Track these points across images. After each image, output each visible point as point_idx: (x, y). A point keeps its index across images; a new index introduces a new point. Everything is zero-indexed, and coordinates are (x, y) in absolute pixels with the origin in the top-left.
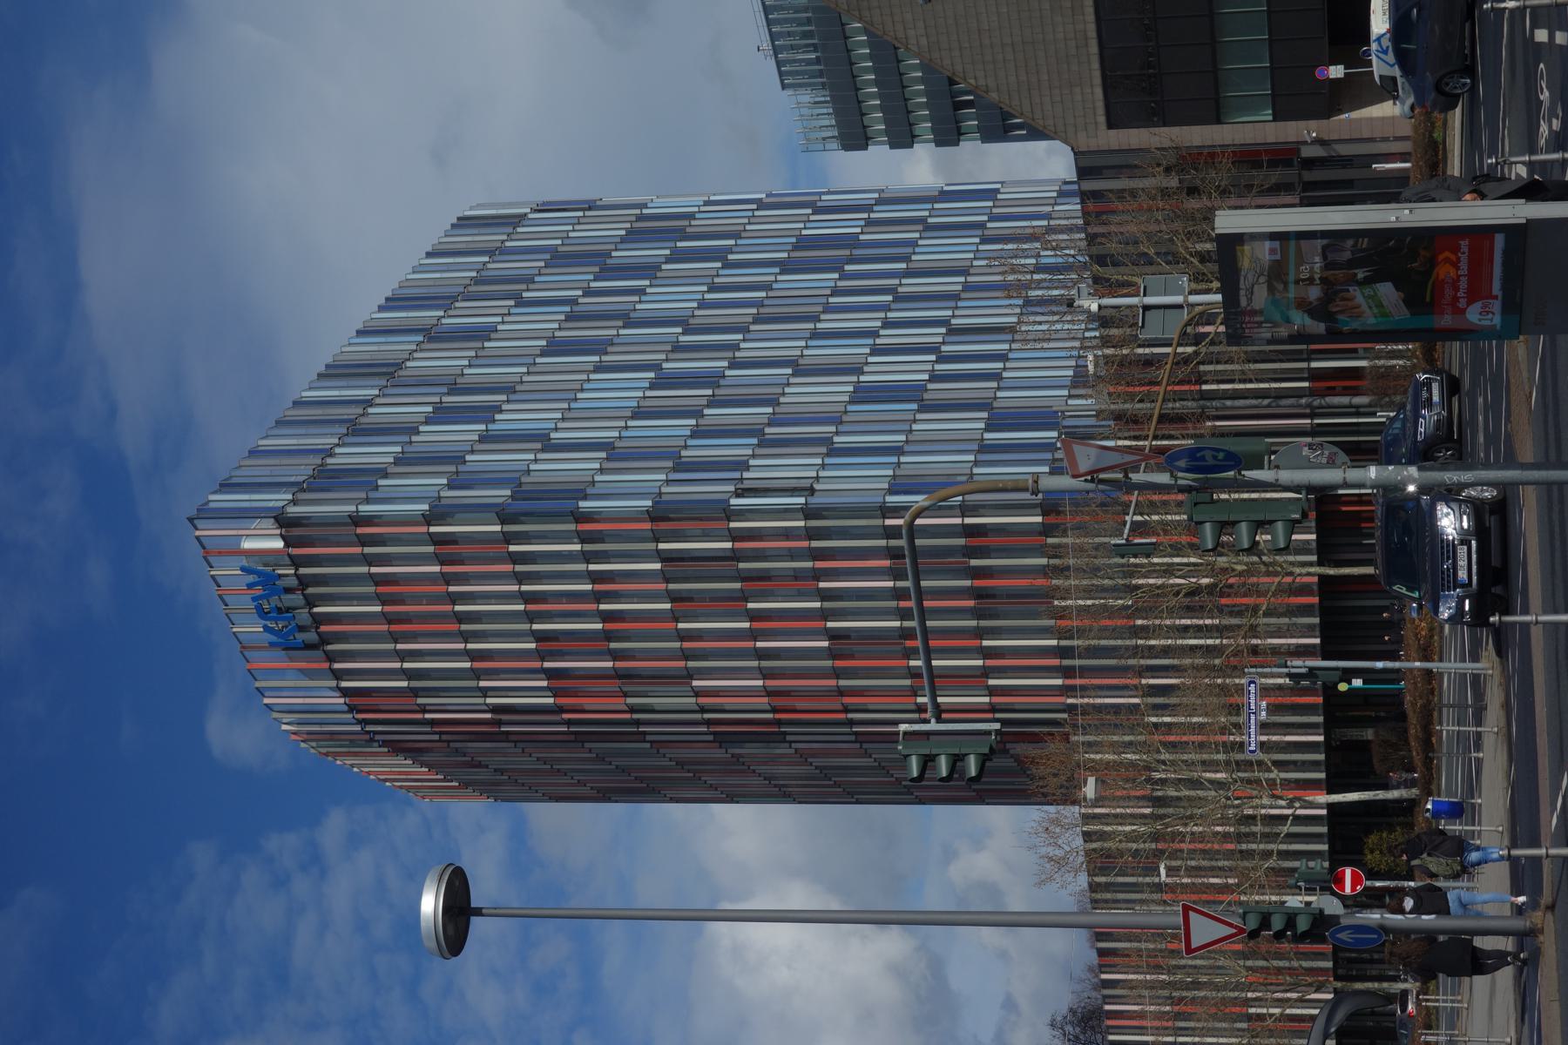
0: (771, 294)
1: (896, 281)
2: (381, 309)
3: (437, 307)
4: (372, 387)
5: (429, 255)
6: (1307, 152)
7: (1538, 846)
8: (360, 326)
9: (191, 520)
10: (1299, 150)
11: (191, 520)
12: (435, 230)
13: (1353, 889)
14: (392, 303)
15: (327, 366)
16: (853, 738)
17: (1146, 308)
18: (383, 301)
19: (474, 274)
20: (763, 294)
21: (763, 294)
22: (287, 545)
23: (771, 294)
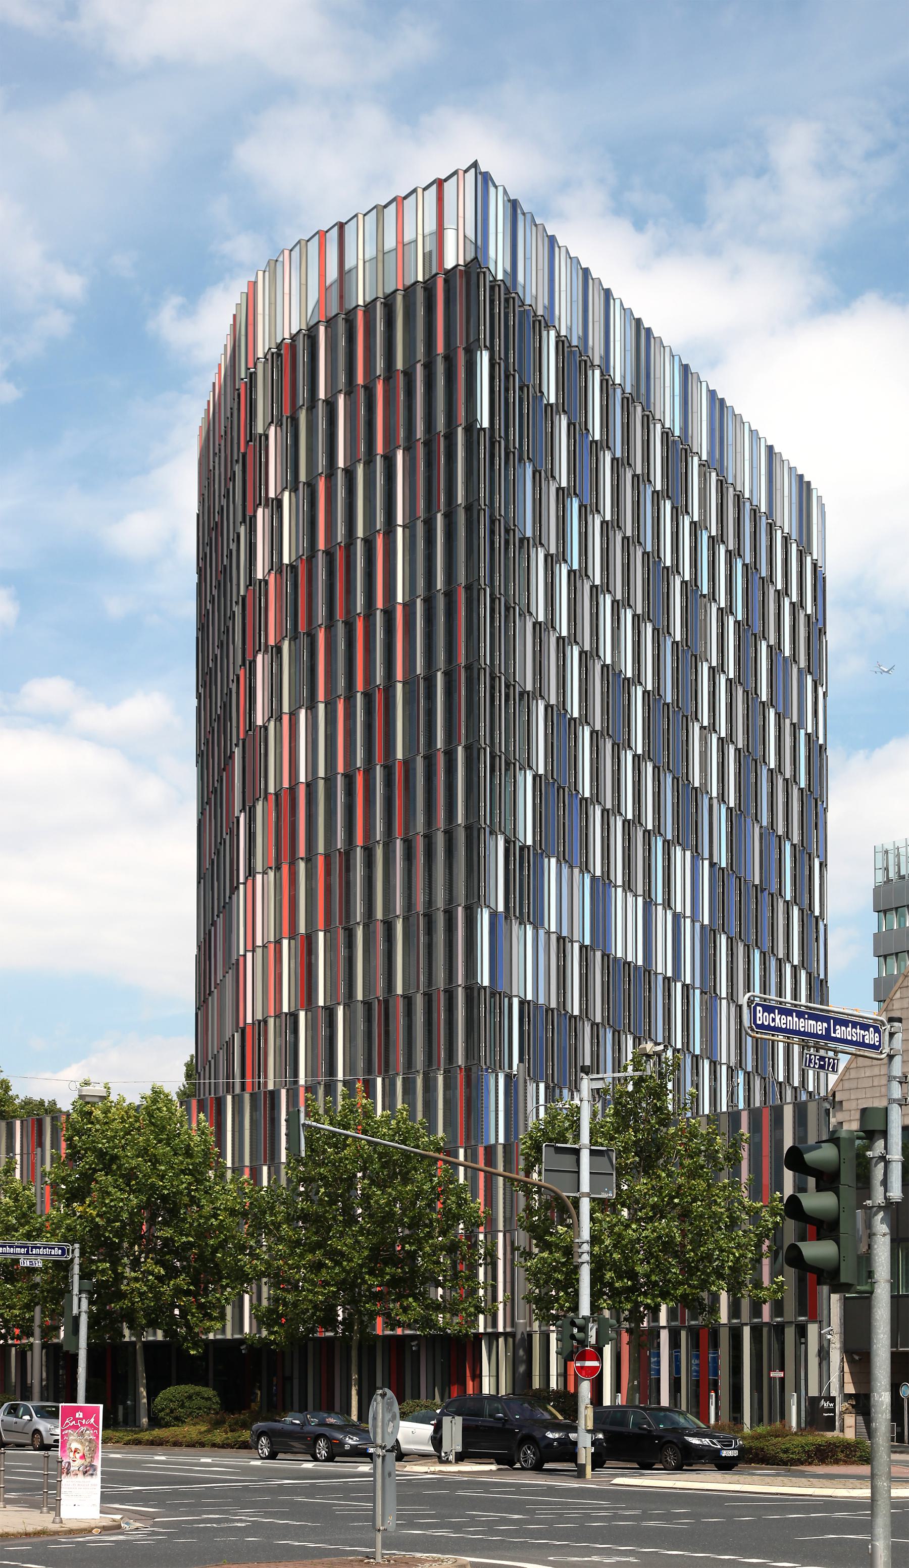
0: (715, 802)
1: (640, 891)
2: (712, 394)
3: (711, 453)
4: (624, 377)
5: (770, 449)
6: (812, 1330)
7: (383, 1547)
8: (777, 450)
9: (475, 165)
10: (815, 1322)
11: (475, 165)
12: (797, 455)
13: (614, 1398)
14: (718, 405)
15: (809, 483)
16: (250, 882)
17: (577, 1152)
18: (806, 479)
19: (747, 495)
20: (714, 794)
21: (714, 794)
22: (447, 273)
23: (715, 802)
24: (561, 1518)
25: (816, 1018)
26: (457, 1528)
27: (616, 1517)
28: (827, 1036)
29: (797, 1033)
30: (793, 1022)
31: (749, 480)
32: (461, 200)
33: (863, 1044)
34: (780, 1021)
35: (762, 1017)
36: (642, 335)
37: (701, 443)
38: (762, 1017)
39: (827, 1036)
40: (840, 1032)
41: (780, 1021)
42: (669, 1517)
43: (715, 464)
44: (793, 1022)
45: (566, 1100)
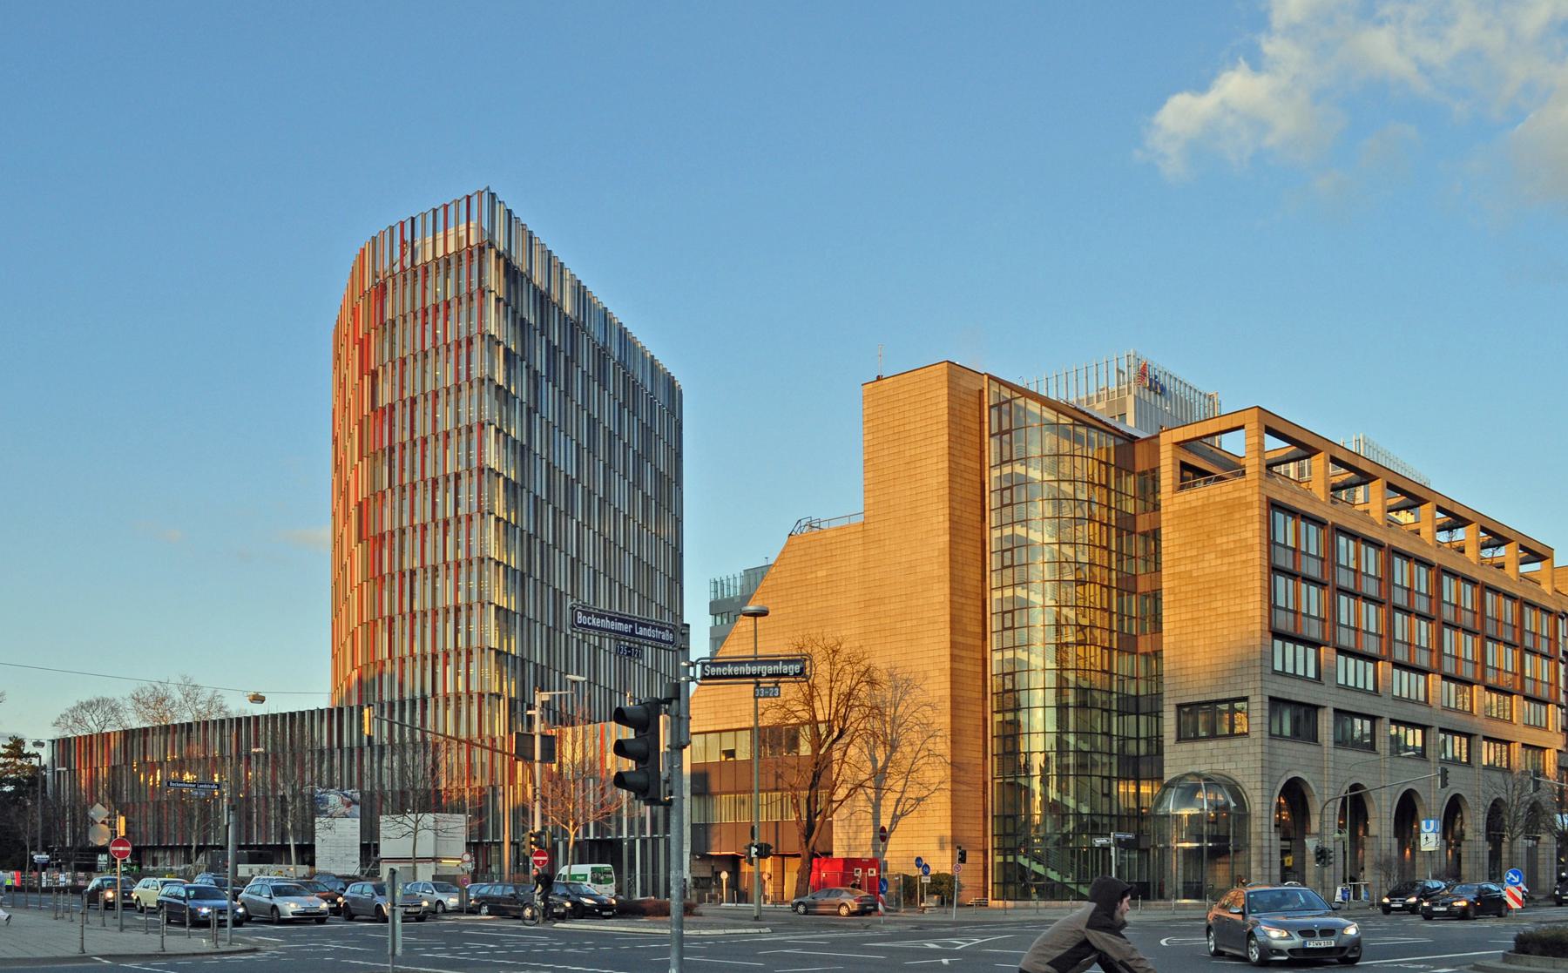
12: (667, 363)
24: (518, 948)
25: (624, 621)
26: (455, 953)
27: (552, 946)
28: (632, 633)
29: (609, 630)
30: (606, 623)
31: (641, 374)
32: (480, 209)
33: (660, 640)
34: (596, 622)
35: (581, 618)
36: (581, 293)
37: (615, 350)
38: (581, 618)
39: (632, 633)
40: (642, 631)
41: (596, 622)
42: (581, 946)
43: (621, 363)
44: (606, 623)
45: (1065, 761)
